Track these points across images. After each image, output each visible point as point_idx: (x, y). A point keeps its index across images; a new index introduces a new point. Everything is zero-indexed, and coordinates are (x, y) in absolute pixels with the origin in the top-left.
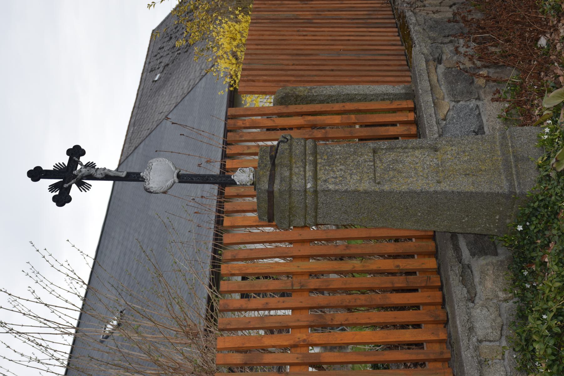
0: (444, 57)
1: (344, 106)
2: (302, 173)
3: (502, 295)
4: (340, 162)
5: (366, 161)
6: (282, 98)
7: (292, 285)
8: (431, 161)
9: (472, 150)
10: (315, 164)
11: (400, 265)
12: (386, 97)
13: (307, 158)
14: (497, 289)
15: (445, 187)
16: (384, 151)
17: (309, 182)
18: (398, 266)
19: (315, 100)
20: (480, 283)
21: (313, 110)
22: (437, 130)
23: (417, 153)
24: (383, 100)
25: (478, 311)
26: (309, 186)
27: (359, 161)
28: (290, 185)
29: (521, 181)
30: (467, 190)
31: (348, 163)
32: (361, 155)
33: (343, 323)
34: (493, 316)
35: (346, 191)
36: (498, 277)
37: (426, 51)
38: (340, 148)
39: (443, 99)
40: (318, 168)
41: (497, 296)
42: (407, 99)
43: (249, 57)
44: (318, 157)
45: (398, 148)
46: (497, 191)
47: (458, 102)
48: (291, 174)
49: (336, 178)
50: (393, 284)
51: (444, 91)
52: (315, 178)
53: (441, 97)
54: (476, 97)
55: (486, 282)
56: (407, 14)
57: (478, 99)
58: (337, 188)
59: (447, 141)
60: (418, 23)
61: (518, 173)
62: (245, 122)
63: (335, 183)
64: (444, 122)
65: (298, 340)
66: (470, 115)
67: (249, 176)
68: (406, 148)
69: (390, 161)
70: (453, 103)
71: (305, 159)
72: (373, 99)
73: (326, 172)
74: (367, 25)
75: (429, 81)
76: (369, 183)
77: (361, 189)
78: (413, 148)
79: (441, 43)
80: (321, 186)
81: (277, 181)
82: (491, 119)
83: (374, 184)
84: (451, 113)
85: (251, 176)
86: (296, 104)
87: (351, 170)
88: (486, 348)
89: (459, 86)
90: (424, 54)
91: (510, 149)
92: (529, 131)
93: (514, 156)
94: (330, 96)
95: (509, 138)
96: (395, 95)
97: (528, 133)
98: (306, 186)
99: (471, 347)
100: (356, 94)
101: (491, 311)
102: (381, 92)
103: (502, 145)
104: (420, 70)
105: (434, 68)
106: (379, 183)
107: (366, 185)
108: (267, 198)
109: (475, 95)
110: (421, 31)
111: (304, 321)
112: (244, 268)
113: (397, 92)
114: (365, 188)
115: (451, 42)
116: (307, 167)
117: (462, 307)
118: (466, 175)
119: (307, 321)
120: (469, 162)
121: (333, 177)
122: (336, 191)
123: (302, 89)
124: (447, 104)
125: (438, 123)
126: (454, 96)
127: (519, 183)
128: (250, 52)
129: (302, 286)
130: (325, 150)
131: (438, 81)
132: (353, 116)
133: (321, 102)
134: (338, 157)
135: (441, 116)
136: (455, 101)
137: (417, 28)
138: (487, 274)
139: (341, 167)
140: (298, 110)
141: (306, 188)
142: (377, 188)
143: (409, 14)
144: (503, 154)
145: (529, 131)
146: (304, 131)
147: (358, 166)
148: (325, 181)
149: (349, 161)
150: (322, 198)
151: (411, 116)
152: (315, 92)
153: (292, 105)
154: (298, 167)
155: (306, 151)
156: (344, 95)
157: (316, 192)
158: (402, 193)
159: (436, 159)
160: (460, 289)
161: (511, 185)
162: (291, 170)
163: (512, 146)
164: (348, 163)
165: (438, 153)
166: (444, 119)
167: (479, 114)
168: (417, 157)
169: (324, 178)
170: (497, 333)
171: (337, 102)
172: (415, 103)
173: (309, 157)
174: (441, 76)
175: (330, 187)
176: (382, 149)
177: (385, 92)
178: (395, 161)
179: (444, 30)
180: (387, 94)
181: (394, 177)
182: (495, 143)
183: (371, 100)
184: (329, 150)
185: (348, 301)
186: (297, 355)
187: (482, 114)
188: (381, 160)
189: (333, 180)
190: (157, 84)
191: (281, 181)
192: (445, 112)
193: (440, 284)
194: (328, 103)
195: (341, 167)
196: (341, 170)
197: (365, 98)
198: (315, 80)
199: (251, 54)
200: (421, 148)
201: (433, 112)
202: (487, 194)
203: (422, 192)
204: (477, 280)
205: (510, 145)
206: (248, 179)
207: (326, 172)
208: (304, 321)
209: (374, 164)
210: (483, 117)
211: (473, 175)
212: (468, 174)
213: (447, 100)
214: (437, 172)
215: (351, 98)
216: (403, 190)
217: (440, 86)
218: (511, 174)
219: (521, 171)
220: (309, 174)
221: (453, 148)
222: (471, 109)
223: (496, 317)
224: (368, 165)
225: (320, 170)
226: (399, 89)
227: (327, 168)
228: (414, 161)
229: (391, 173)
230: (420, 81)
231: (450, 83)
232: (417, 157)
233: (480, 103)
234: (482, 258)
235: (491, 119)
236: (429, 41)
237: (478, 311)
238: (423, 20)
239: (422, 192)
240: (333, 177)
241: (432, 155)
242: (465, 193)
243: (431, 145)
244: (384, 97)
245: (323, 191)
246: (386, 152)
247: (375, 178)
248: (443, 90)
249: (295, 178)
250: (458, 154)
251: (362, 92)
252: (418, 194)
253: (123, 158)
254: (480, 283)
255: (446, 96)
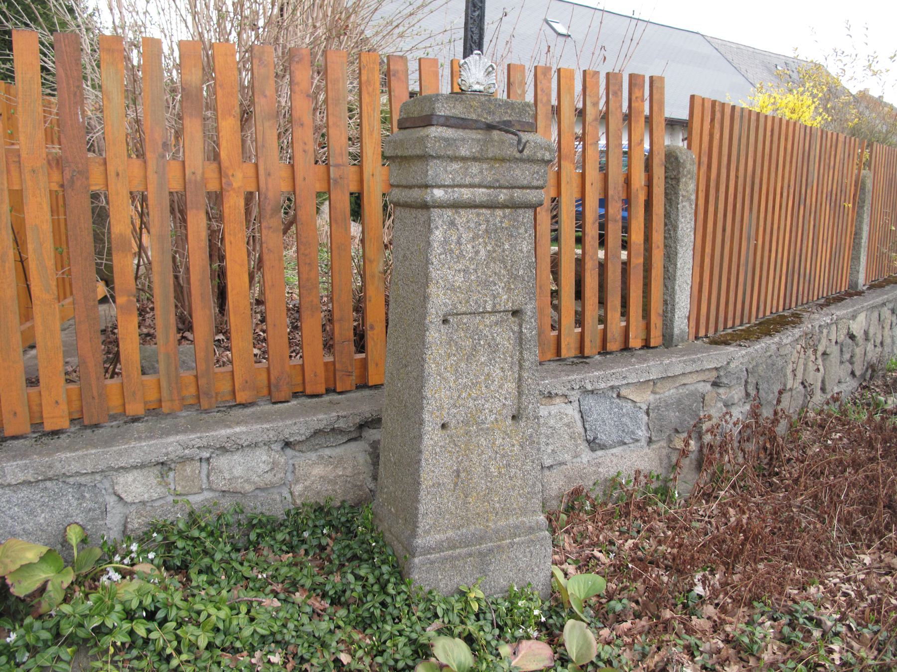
0: (721, 391)
1: (658, 247)
2: (468, 180)
3: (298, 488)
4: (495, 251)
5: (495, 297)
6: (676, 158)
7: (337, 166)
8: (491, 411)
9: (511, 478)
10: (492, 206)
11: (375, 332)
12: (669, 306)
13: (505, 191)
14: (307, 483)
15: (431, 437)
16: (516, 329)
17: (446, 193)
18: (372, 328)
19: (671, 206)
20: (321, 457)
21: (654, 202)
22: (598, 387)
23: (511, 386)
24: (665, 302)
25: (264, 458)
26: (438, 193)
27: (495, 284)
28: (438, 157)
29: (436, 565)
30: (423, 475)
31: (492, 265)
32: (509, 289)
33: (264, 245)
34: (255, 478)
35: (428, 262)
36: (333, 482)
37: (732, 365)
38: (525, 250)
39: (653, 392)
40: (484, 211)
41: (297, 482)
42: (663, 336)
43: (753, 118)
44: (507, 211)
45: (521, 353)
46: (421, 525)
47: (648, 414)
48: (464, 159)
49: (459, 243)
50: (340, 320)
51: (667, 394)
52: (456, 206)
53: (658, 390)
54: (653, 438)
55: (322, 467)
56: (796, 330)
57: (650, 441)
58: (435, 245)
59: (531, 436)
60: (779, 346)
61: (453, 558)
62: (639, 100)
63: (446, 242)
64: (615, 396)
65: (230, 173)
66: (623, 431)
67: (478, 83)
68: (521, 367)
69: (493, 339)
70: (645, 407)
71: (501, 187)
72: (667, 289)
73: (472, 225)
74: (790, 275)
75: (683, 374)
76: (445, 304)
77: (432, 289)
78: (520, 378)
79: (746, 382)
80: (440, 218)
81: (449, 133)
82: (615, 460)
83: (441, 313)
84: (630, 404)
85: (476, 87)
86: (666, 178)
87: (475, 270)
88: (193, 471)
89: (673, 414)
90: (728, 363)
91: (508, 541)
92: (541, 567)
93: (491, 551)
94: (675, 228)
95: (532, 536)
96: (672, 321)
97: (538, 567)
98: (439, 187)
99: (187, 451)
100: (676, 265)
101: (266, 475)
102: (677, 300)
103: (517, 527)
104: (702, 361)
105: (705, 378)
106: (445, 321)
107: (439, 300)
108: (424, 114)
109: (656, 436)
110: (769, 354)
111: (266, 184)
112: (371, 89)
113: (676, 324)
114: (433, 299)
115: (748, 395)
116: (484, 190)
117: (265, 436)
118: (458, 472)
119: (267, 189)
120: (486, 475)
121: (460, 238)
122: (429, 244)
123: (688, 187)
124: (645, 398)
125: (612, 388)
126: (657, 408)
127: (432, 563)
128: (762, 120)
129: (335, 181)
130: (523, 224)
131: (684, 384)
132: (641, 260)
133: (667, 215)
134: (507, 247)
135: (624, 392)
136: (648, 409)
137: (774, 347)
138: (336, 467)
139: (483, 253)
140: (655, 181)
141: (433, 187)
142: (434, 315)
143: (797, 332)
144: (497, 532)
145: (541, 567)
146: (620, 189)
147: (485, 284)
148: (452, 223)
149: (497, 267)
150: (421, 215)
151: (635, 342)
152: (684, 207)
153: (666, 172)
154: (481, 172)
155: (519, 188)
156: (676, 248)
157: (425, 206)
158: (422, 363)
159: (496, 419)
160: (301, 432)
161: (429, 550)
162: (475, 159)
163: (512, 544)
164: (492, 265)
165: (509, 421)
166: (619, 396)
167: (625, 444)
168: (501, 387)
169: (458, 221)
170: (223, 485)
171: (665, 238)
172: (656, 347)
173: (505, 194)
174: (692, 388)
175: (437, 233)
176: (521, 326)
177: (677, 306)
178: (493, 348)
179: (768, 382)
180: (673, 309)
181: (460, 348)
182: (524, 514)
183: (665, 286)
184: (522, 231)
185: (307, 252)
186: (199, 172)
187: (625, 447)
188: (496, 324)
189: (454, 238)
190: (773, 68)
191: (446, 140)
192: (631, 397)
193: (338, 390)
194: (666, 225)
195: (483, 253)
196: (477, 253)
197: (669, 277)
198: (710, 206)
199: (758, 120)
200: (520, 394)
201: (630, 381)
202: (417, 509)
203: (423, 398)
204: (327, 452)
205: (517, 540)
206: (471, 81)
207: (472, 225)
208: (266, 184)
209: (489, 312)
210: (621, 448)
211: (456, 484)
212: (458, 476)
213: (651, 398)
214: (467, 423)
215: (670, 257)
216: (426, 366)
217: (676, 388)
218: (454, 547)
219: (461, 563)
220: (466, 194)
221: (516, 448)
222: (633, 433)
223: (254, 483)
224: (486, 302)
225: (478, 215)
226: (681, 323)
227: (483, 227)
228: (493, 381)
229: (469, 343)
230: (685, 362)
231: (679, 402)
232: (501, 387)
233: (643, 442)
234: (368, 457)
235: (615, 460)
236: (751, 366)
237: (264, 458)
238: (787, 352)
239: (423, 398)
240: (460, 238)
241: (505, 411)
242: (417, 471)
243: (526, 407)
244: (669, 305)
245: (429, 221)
246: (514, 333)
247: (457, 314)
248: (669, 392)
249: (455, 166)
250: (503, 456)
251: (679, 273)
252: (420, 390)
253: (709, 39)
254: (321, 457)
255: (658, 396)
